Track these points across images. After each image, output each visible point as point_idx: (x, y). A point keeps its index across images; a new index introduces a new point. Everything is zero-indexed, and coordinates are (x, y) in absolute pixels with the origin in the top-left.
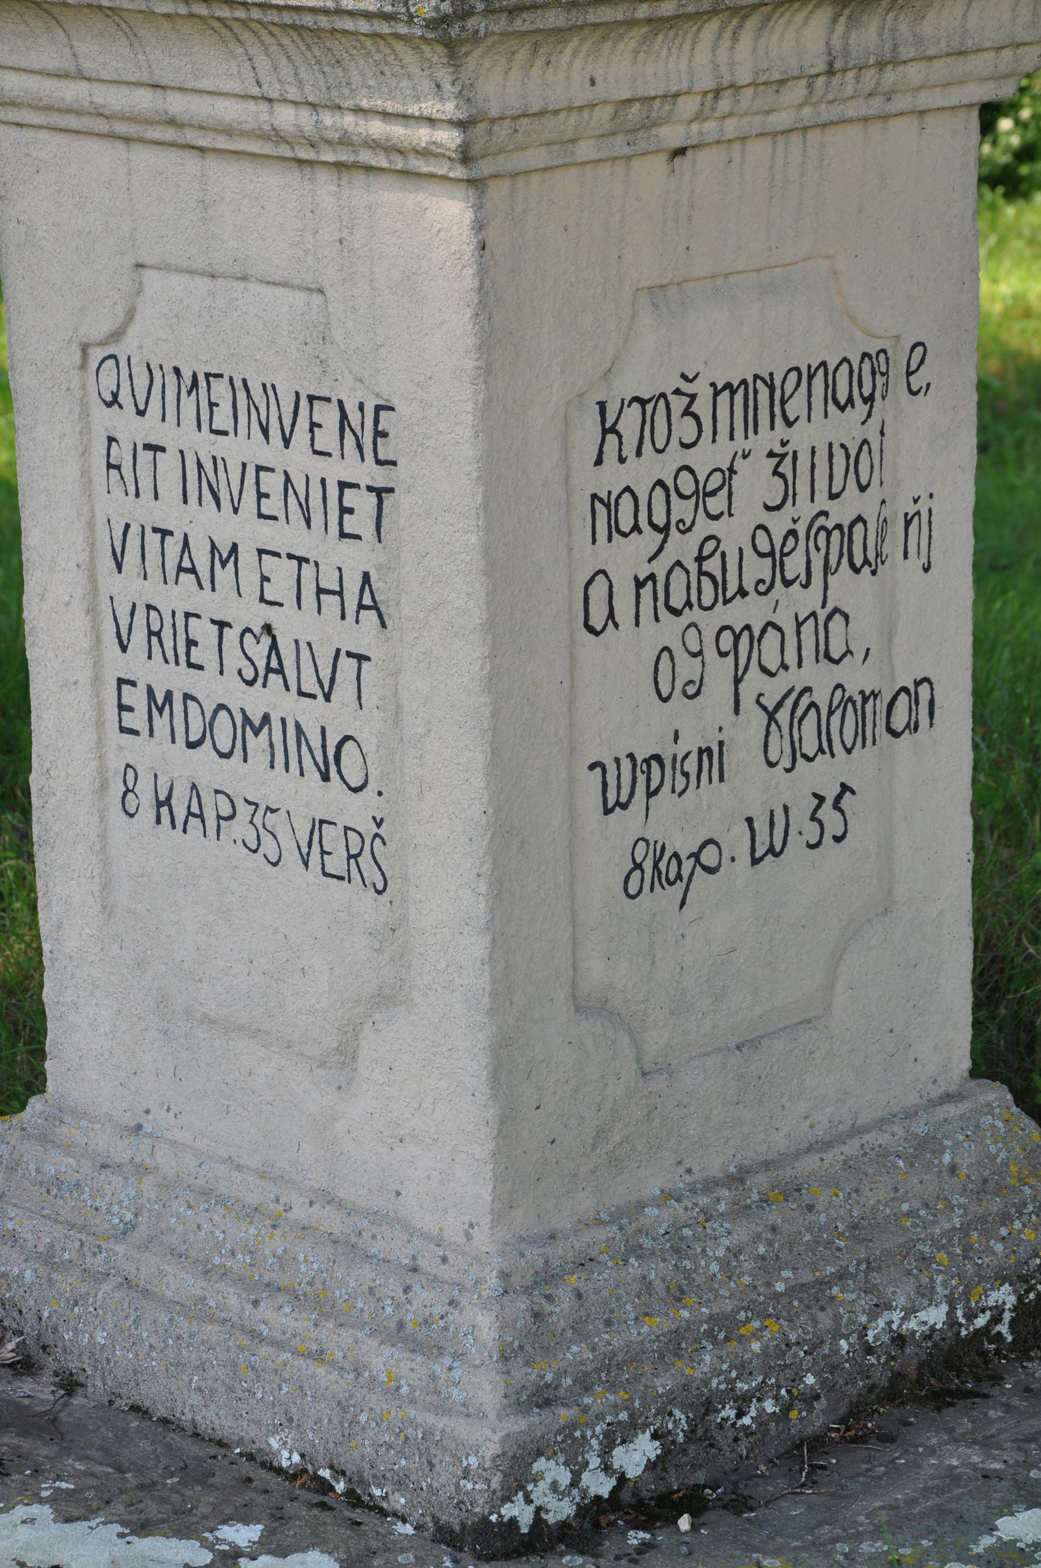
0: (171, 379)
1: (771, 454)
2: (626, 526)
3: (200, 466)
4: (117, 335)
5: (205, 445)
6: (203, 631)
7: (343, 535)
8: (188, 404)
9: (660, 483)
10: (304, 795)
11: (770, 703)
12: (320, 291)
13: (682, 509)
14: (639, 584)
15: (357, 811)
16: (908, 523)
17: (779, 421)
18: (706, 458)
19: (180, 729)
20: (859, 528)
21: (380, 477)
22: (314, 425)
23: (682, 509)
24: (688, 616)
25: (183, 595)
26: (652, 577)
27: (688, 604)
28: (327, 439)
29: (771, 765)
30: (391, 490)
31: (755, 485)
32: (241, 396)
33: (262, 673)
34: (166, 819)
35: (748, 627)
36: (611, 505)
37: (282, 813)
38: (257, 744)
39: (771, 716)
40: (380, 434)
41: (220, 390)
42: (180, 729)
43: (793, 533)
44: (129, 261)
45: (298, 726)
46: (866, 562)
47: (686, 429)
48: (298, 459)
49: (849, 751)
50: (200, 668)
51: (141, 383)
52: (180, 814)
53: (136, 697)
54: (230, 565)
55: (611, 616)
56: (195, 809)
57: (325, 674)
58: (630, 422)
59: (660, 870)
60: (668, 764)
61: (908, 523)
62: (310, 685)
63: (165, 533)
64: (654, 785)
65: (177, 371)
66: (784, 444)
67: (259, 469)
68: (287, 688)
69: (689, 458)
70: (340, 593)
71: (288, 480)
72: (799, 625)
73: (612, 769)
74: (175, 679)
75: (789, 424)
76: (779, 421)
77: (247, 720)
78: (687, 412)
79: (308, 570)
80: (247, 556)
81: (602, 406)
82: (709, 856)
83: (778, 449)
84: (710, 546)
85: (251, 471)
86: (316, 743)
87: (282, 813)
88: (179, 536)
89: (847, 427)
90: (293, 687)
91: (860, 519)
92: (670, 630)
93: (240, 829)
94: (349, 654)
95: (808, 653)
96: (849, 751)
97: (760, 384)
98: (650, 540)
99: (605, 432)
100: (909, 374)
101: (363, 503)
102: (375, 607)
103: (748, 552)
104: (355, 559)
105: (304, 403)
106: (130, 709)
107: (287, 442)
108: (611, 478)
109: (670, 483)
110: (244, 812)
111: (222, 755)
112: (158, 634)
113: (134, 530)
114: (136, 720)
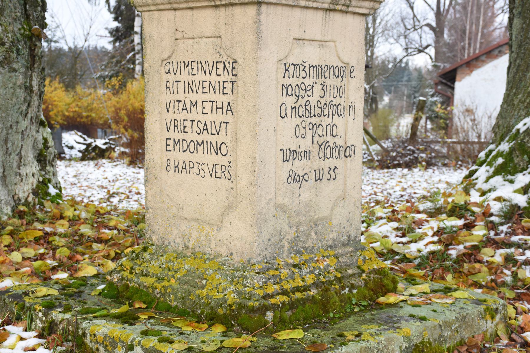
0: (183, 64)
1: (321, 84)
2: (290, 94)
3: (189, 84)
4: (170, 57)
5: (190, 78)
6: (188, 124)
7: (223, 94)
8: (187, 70)
9: (297, 85)
10: (211, 159)
11: (320, 143)
12: (220, 37)
13: (302, 93)
14: (292, 108)
15: (225, 161)
16: (350, 108)
17: (323, 77)
18: (308, 81)
19: (181, 148)
20: (339, 106)
21: (234, 78)
22: (217, 68)
23: (302, 93)
24: (303, 118)
25: (184, 115)
26: (295, 107)
27: (303, 115)
28: (220, 72)
29: (320, 158)
30: (236, 82)
31: (317, 91)
32: (200, 65)
33: (202, 131)
34: (177, 171)
35: (315, 124)
36: (287, 88)
37: (206, 164)
38: (200, 149)
39: (320, 146)
40: (233, 68)
41: (195, 65)
42: (181, 148)
43: (326, 104)
44: (174, 38)
45: (211, 142)
46: (341, 115)
47: (303, 74)
48: (213, 78)
49: (337, 159)
50: (187, 132)
51: (175, 67)
52: (180, 168)
53: (171, 142)
54: (195, 106)
55: (286, 114)
56: (184, 167)
57: (218, 128)
58: (291, 69)
59: (296, 178)
60: (298, 153)
61: (350, 108)
62: (214, 131)
63: (180, 101)
64: (294, 157)
65: (184, 62)
66: (324, 83)
67: (203, 81)
68: (208, 133)
69: (304, 81)
70: (222, 108)
71: (210, 83)
72: (327, 126)
73: (285, 151)
74: (181, 136)
75: (325, 78)
76: (323, 77)
77: (198, 143)
78: (303, 70)
79: (214, 104)
80: (200, 103)
81: (285, 64)
82: (306, 177)
83: (323, 83)
84: (308, 103)
85: (201, 83)
86: (215, 145)
87: (206, 164)
88: (183, 102)
89: (337, 82)
90: (210, 133)
91: (340, 104)
92: (299, 121)
93: (195, 170)
94: (224, 122)
95: (328, 133)
96: (337, 159)
97: (319, 68)
98: (294, 98)
99: (286, 70)
100: (351, 73)
101: (229, 85)
102: (231, 110)
103: (316, 106)
104: (225, 99)
105: (215, 64)
106: (169, 145)
107: (210, 74)
108: (287, 82)
109: (300, 86)
110: (196, 165)
111: (191, 153)
112: (177, 126)
113: (172, 102)
114: (171, 148)
